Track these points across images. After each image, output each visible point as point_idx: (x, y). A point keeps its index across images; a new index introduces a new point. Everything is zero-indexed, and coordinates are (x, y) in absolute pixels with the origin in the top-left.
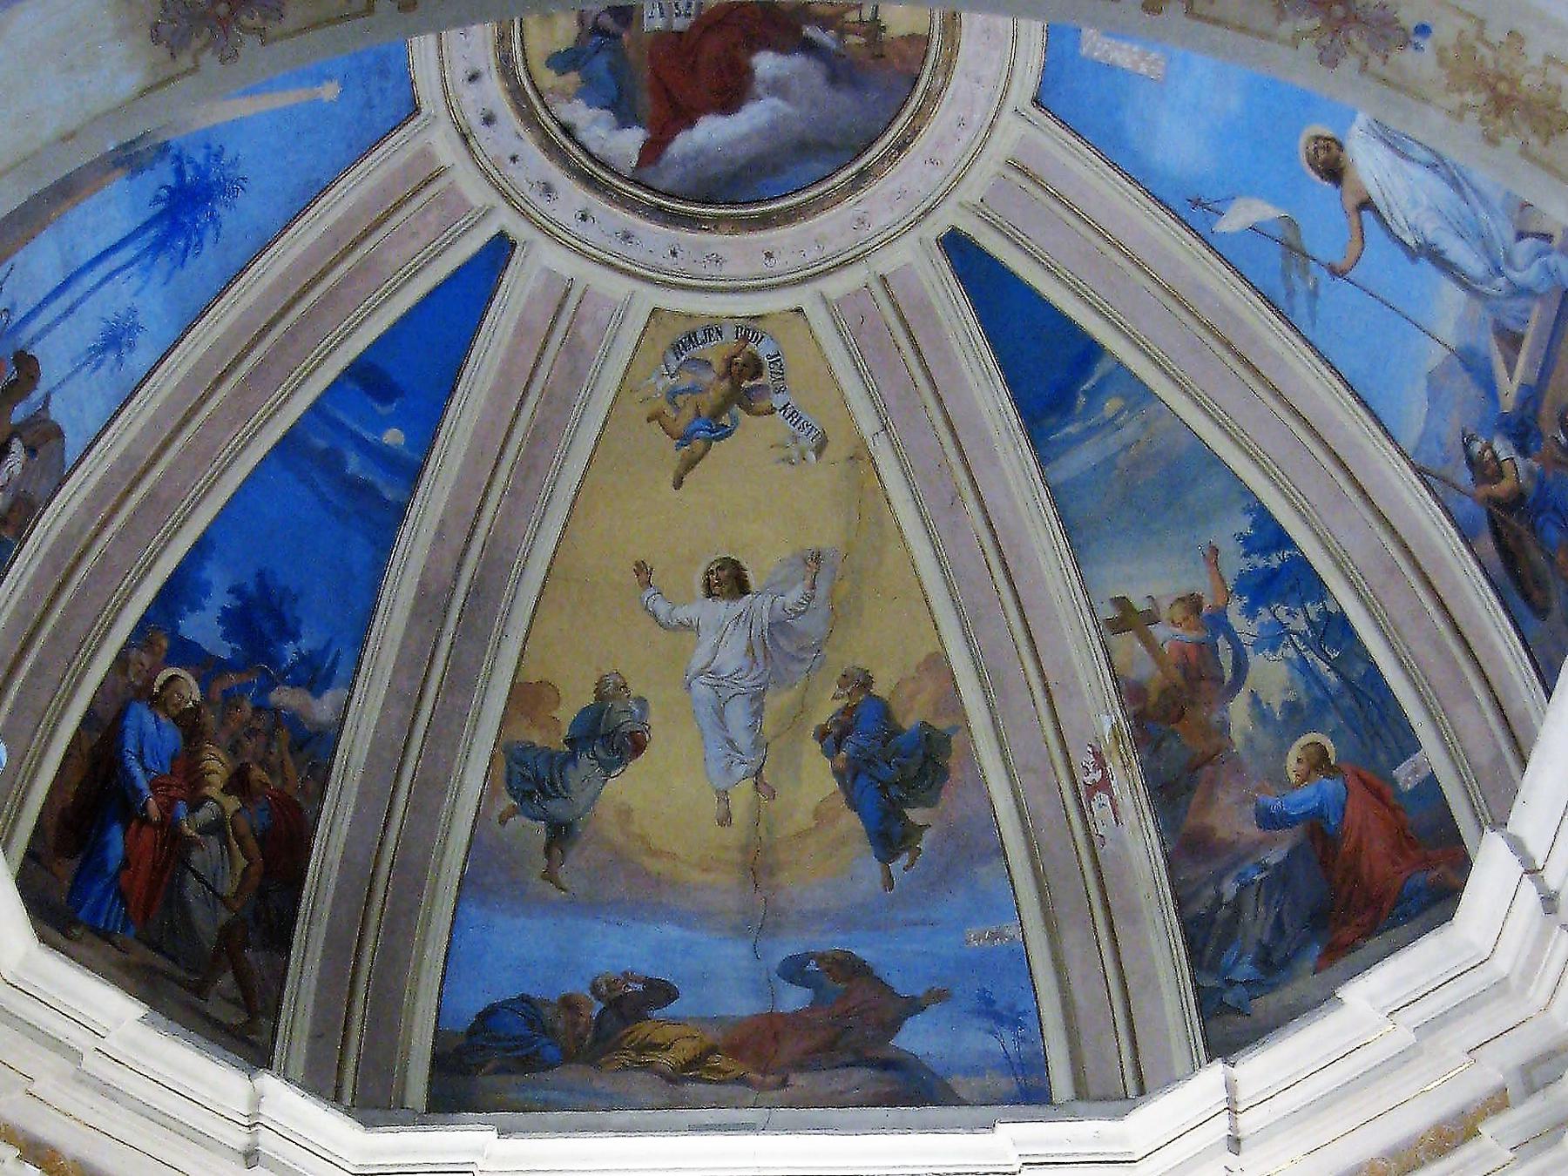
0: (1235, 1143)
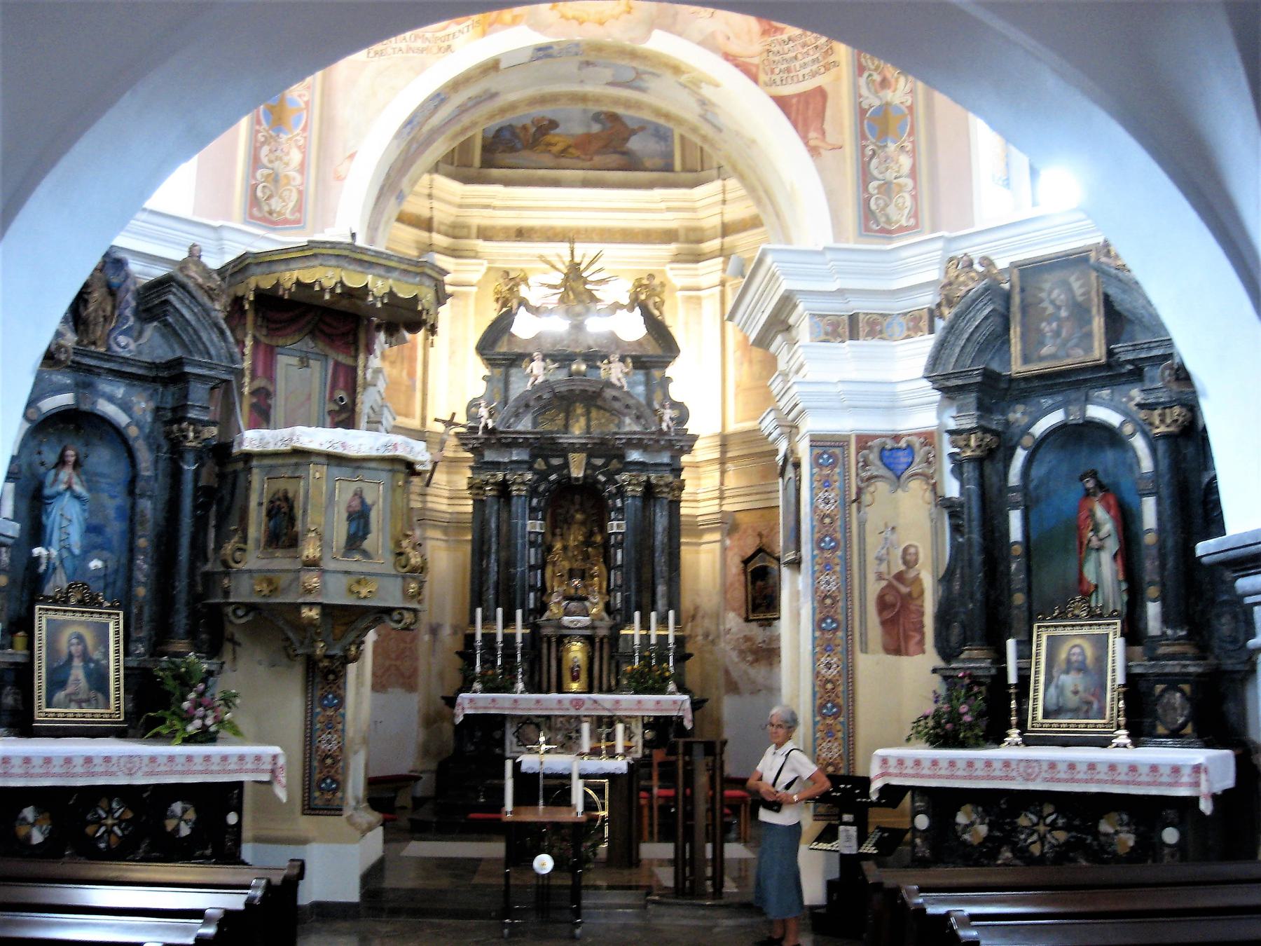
0: (724, 202)
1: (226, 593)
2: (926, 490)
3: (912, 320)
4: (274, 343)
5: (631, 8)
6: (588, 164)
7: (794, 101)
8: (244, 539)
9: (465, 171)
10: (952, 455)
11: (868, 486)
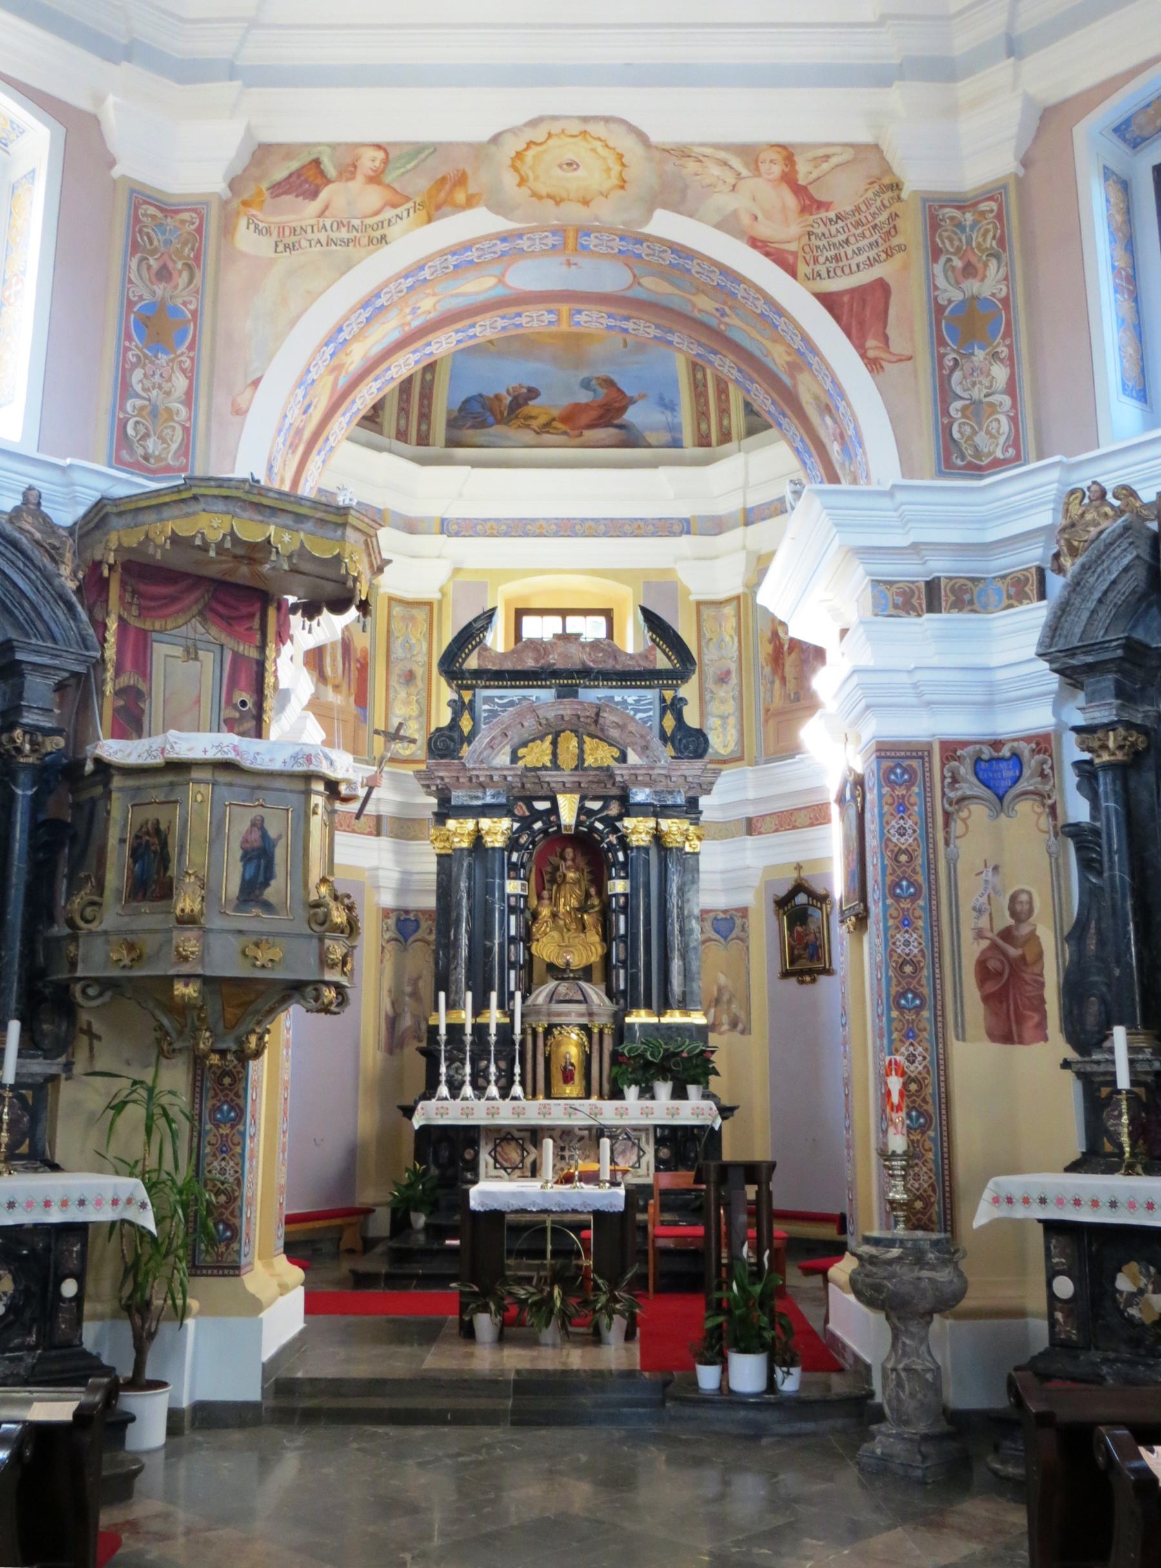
1: (73, 965)
2: (1040, 815)
3: (1013, 585)
4: (147, 626)
5: (624, 181)
6: (578, 441)
7: (846, 299)
8: (100, 888)
9: (422, 450)
10: (1078, 765)
11: (958, 811)
